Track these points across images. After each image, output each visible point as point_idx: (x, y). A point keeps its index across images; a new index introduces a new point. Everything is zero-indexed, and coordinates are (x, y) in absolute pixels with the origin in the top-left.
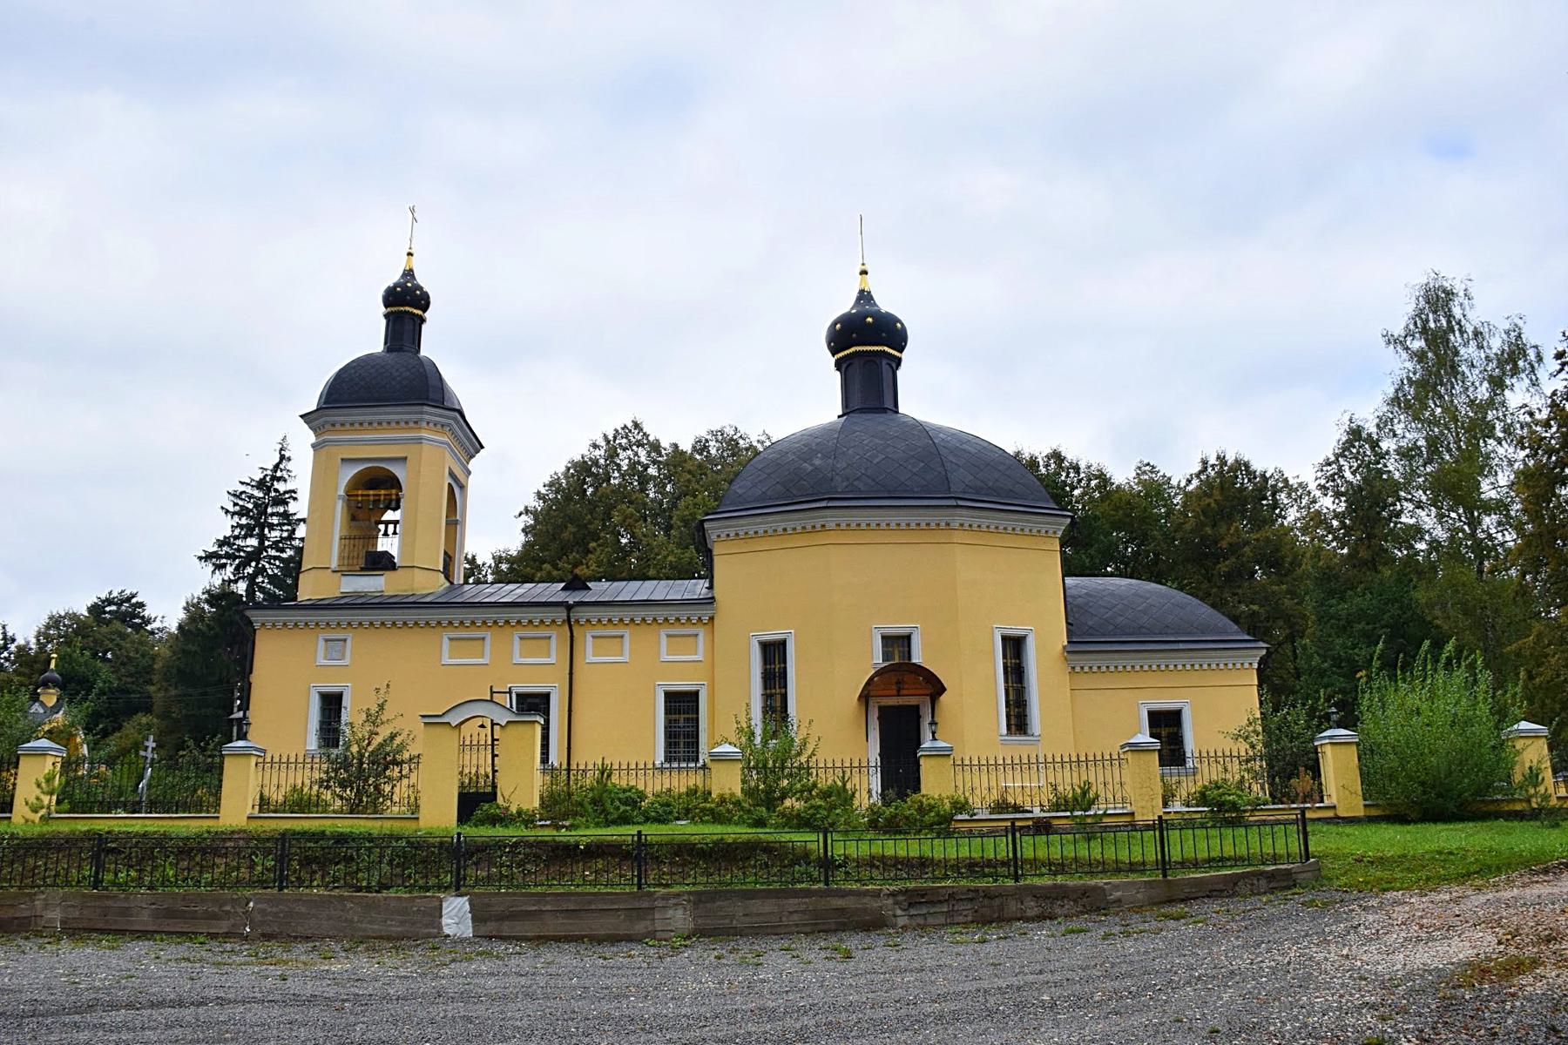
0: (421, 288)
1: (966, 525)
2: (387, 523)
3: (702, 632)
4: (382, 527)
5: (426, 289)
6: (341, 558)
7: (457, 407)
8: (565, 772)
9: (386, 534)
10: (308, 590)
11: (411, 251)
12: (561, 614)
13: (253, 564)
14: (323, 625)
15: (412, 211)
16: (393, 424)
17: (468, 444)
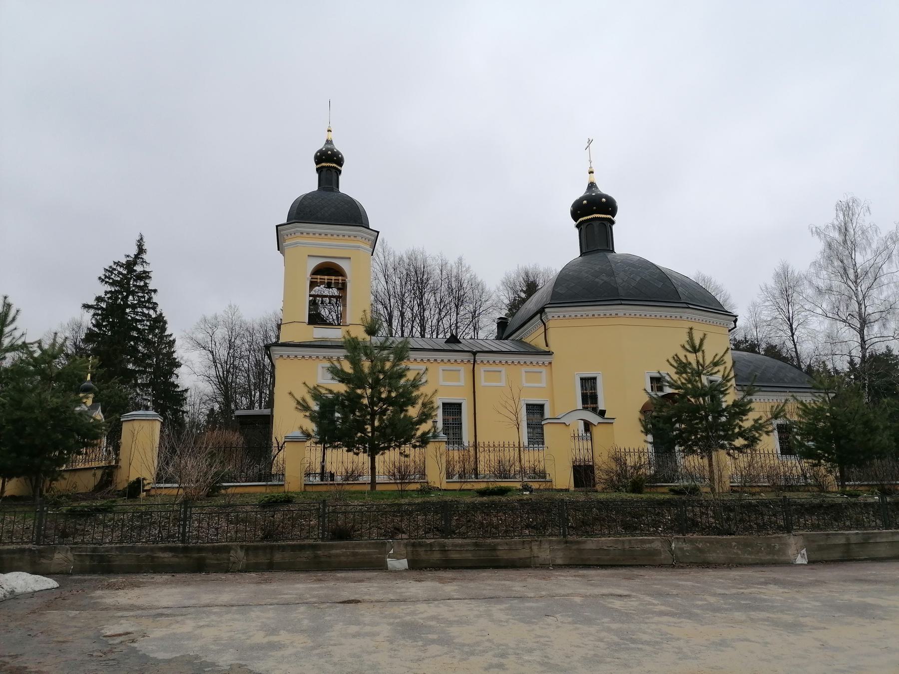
1: (658, 316)
3: (544, 370)
11: (330, 129)
12: (467, 357)
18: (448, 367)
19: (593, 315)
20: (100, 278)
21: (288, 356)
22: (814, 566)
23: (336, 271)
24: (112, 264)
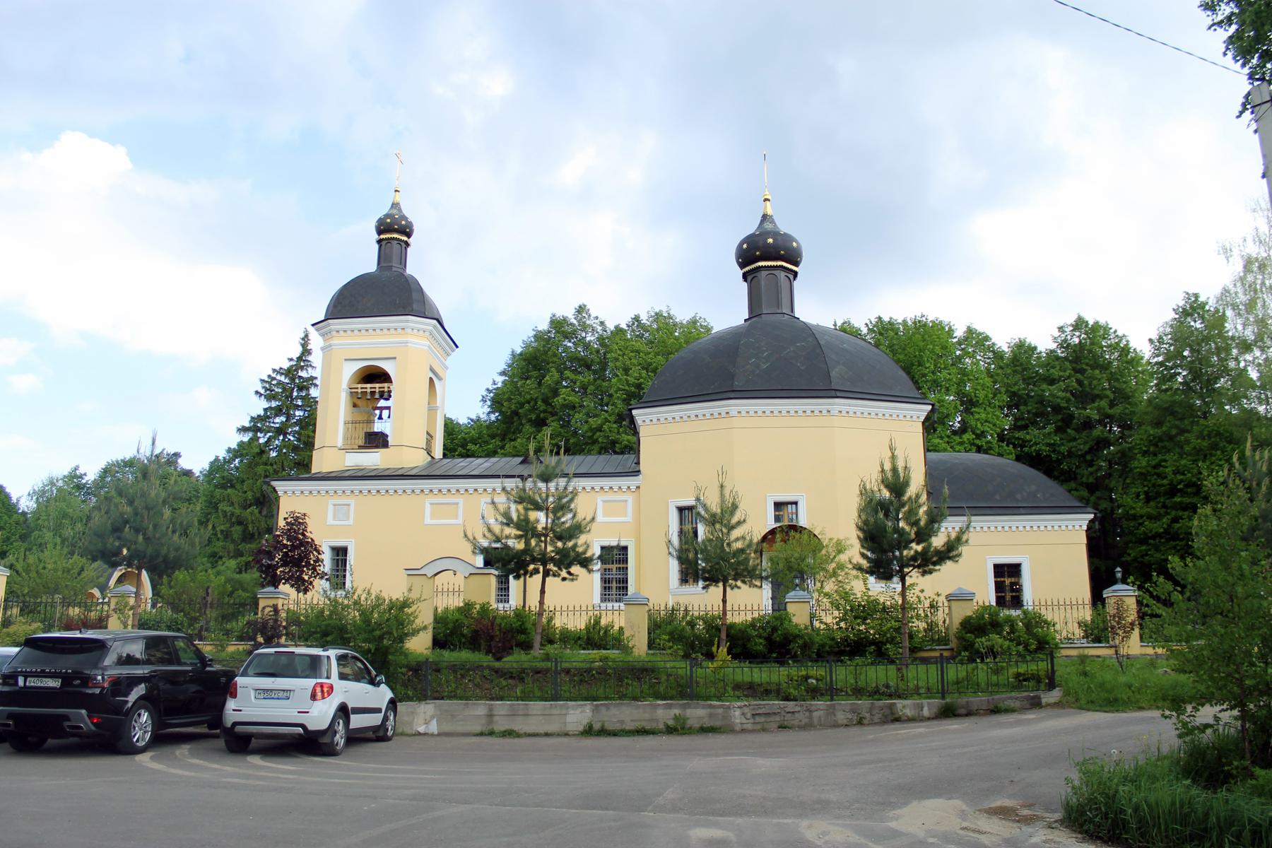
0: (405, 218)
2: (381, 409)
3: (630, 498)
4: (377, 412)
5: (411, 218)
6: (345, 438)
7: (436, 317)
8: (728, 609)
9: (380, 418)
10: (322, 461)
13: (281, 438)
14: (331, 493)
16: (378, 331)
17: (447, 348)
18: (440, 499)
19: (796, 412)
20: (257, 392)
21: (378, 491)
22: (166, 750)
23: (382, 376)
24: (271, 373)
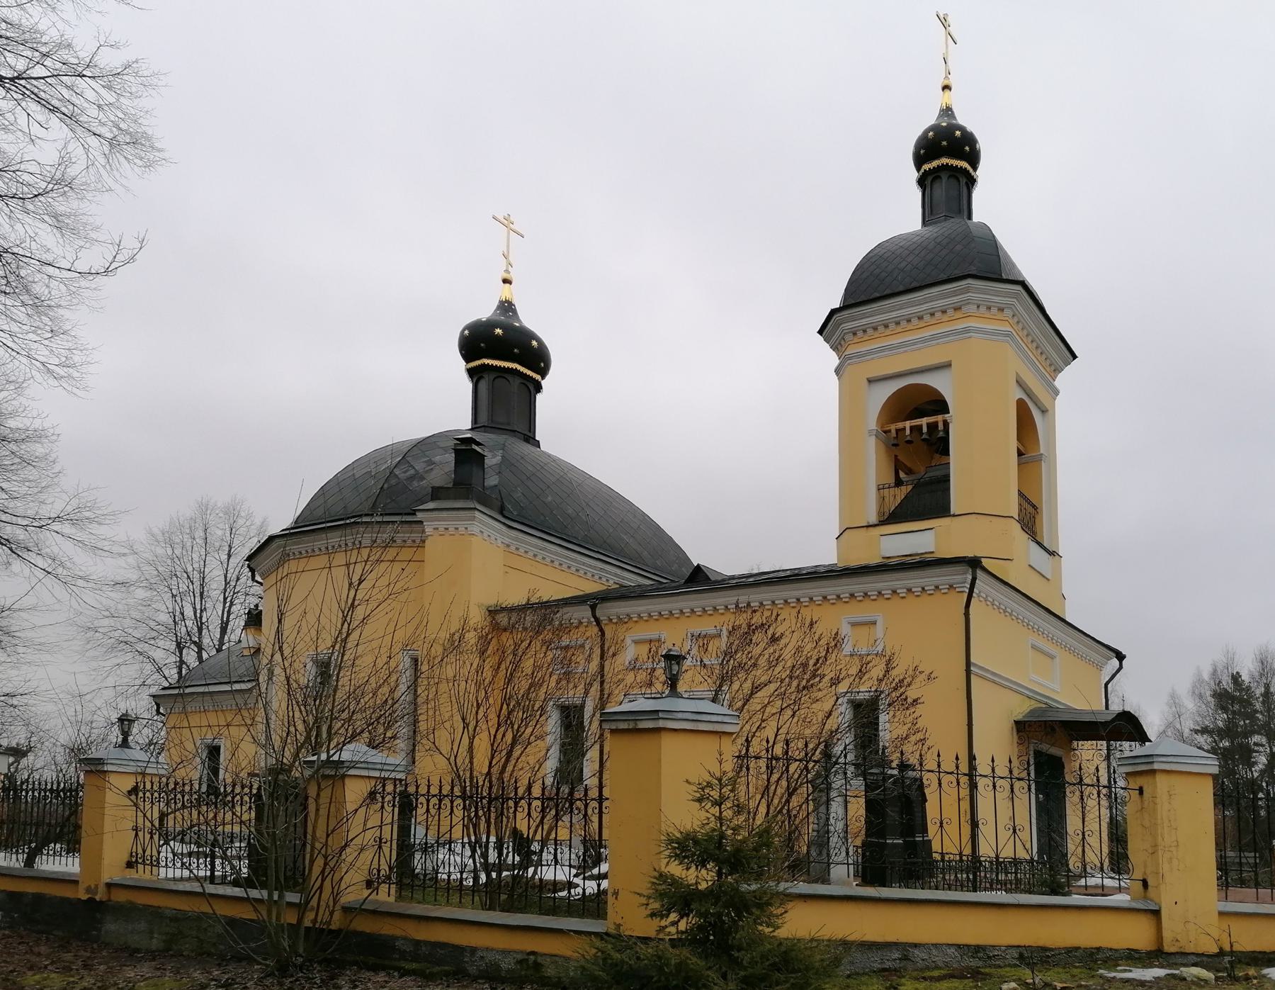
0: (962, 129)
5: (970, 128)
15: (944, 21)
